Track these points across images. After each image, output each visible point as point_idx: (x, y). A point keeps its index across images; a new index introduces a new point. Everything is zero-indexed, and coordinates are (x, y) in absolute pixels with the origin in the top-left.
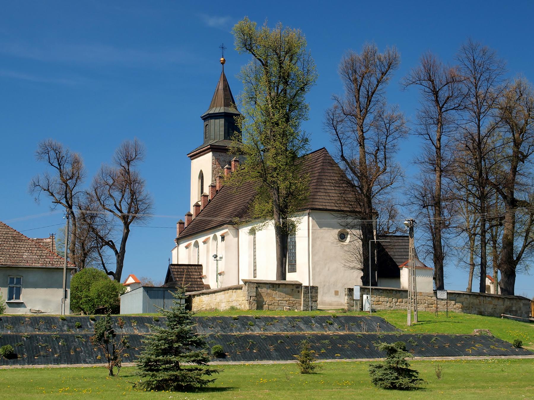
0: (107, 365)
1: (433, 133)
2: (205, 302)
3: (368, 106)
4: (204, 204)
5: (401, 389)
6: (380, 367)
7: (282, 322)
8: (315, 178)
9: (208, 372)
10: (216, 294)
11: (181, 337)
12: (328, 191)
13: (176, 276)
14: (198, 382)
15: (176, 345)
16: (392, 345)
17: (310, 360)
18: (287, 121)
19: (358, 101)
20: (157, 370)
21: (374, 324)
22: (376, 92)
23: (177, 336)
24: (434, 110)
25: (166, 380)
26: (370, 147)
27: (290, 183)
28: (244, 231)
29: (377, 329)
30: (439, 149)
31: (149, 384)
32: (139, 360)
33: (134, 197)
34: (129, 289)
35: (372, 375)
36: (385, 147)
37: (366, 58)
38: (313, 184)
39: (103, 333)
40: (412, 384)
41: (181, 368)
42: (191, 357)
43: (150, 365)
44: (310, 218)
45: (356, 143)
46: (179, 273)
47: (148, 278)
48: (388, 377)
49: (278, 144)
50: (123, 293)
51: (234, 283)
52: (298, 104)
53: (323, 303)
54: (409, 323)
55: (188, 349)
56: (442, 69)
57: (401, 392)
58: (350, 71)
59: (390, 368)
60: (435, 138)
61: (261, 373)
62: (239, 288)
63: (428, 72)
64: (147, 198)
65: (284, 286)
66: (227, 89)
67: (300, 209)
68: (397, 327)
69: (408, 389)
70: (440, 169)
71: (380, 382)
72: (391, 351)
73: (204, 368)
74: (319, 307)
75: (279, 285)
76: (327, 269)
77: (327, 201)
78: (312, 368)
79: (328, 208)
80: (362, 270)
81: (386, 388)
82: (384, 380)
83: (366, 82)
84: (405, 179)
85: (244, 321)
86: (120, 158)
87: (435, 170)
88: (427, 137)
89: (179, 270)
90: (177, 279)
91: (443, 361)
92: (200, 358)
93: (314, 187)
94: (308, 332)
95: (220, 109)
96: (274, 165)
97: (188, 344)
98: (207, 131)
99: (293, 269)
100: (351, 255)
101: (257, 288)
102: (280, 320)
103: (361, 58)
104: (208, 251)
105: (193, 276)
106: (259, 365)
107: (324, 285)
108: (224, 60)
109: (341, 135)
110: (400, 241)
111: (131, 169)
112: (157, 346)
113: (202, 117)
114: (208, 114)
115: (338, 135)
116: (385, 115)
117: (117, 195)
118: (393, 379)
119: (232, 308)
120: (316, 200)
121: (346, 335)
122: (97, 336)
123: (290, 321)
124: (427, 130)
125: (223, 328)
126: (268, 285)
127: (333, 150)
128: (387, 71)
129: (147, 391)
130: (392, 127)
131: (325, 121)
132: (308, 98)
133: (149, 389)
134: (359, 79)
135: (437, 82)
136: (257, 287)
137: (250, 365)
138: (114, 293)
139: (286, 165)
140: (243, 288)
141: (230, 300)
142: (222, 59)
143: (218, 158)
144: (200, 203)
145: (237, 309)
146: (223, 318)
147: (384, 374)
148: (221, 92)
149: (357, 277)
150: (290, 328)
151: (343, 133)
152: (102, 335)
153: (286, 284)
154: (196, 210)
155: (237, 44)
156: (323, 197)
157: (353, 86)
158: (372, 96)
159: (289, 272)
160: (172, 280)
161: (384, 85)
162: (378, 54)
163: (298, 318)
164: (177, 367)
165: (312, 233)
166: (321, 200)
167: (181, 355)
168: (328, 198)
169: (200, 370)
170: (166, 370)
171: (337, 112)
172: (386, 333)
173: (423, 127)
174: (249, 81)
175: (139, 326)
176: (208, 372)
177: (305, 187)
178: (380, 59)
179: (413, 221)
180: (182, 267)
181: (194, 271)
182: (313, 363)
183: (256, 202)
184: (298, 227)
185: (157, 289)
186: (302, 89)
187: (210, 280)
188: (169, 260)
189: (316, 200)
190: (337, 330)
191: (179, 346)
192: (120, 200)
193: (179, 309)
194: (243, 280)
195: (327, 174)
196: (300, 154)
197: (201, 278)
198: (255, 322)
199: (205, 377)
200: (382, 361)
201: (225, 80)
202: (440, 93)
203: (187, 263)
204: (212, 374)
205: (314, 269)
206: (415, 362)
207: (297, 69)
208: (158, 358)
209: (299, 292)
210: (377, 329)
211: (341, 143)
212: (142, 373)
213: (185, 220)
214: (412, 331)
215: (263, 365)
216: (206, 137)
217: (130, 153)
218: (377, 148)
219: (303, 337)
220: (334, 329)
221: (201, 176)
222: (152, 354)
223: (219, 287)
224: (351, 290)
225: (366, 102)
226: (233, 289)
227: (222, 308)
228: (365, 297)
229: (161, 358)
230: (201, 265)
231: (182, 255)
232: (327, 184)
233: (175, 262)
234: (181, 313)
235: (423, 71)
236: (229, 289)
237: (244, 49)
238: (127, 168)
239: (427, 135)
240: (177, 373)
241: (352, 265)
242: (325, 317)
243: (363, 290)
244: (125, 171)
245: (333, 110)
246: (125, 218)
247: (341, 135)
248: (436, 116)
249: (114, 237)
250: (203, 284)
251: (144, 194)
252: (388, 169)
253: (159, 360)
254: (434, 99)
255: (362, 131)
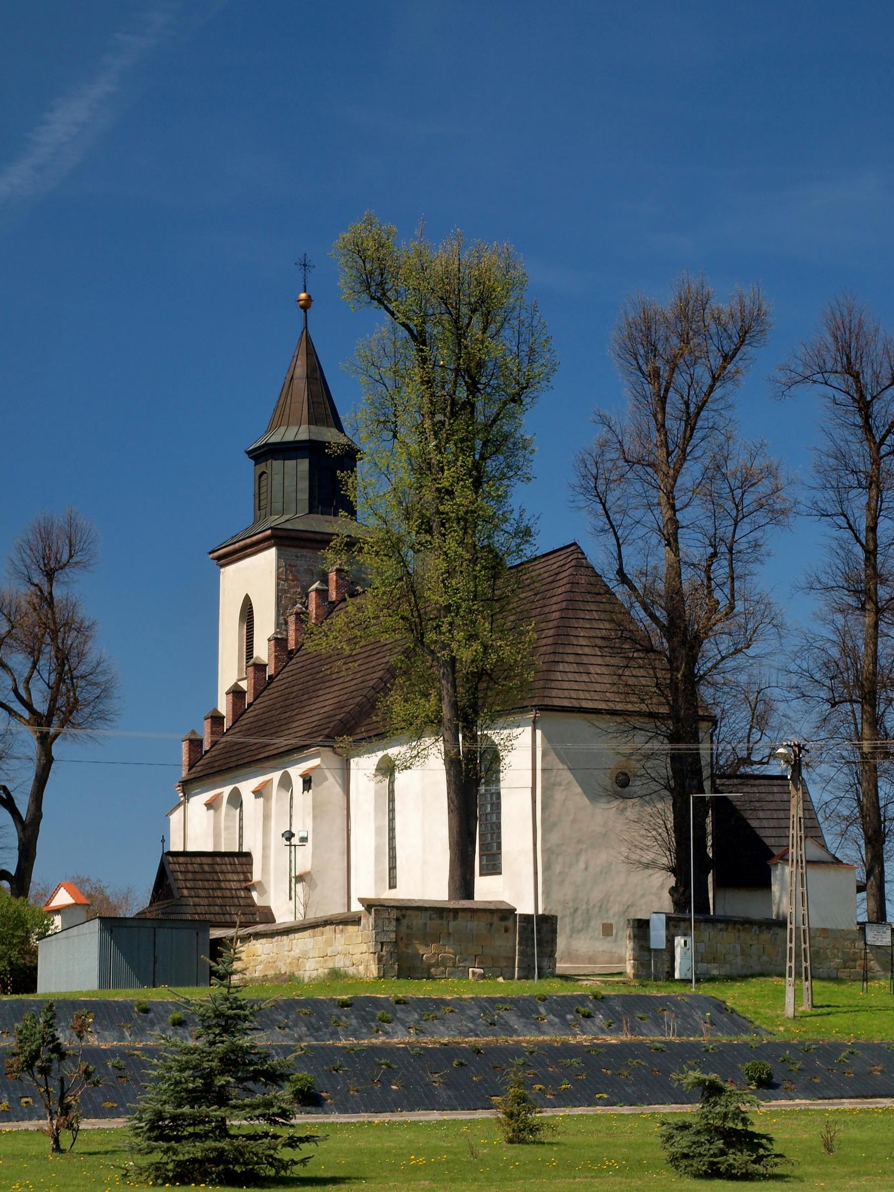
0: (45, 1124)
1: (857, 513)
2: (264, 957)
3: (687, 439)
4: (255, 689)
5: (730, 1176)
6: (684, 1127)
7: (462, 1011)
8: (551, 625)
9: (293, 1142)
10: (292, 936)
11: (233, 1061)
12: (585, 660)
13: (182, 884)
14: (271, 1165)
15: (220, 1081)
16: (713, 1076)
17: (530, 1111)
18: (477, 484)
19: (661, 427)
20: (178, 1139)
21: (697, 1015)
22: (709, 405)
23: (221, 1060)
24: (858, 451)
25: (194, 1161)
26: (693, 548)
27: (485, 647)
28: (363, 766)
29: (704, 1027)
30: (871, 553)
31: (158, 1167)
32: (137, 1115)
33: (67, 668)
34: (58, 920)
35: (667, 1146)
36: (730, 550)
37: (683, 315)
38: (544, 642)
39: (37, 1051)
40: (757, 1166)
41: (232, 1132)
42: (254, 1107)
43: (160, 1127)
44: (539, 733)
45: (655, 538)
46: (190, 876)
47: (94, 879)
48: (701, 1150)
49: (454, 545)
50: (42, 936)
51: (336, 909)
52: (506, 437)
53: (571, 956)
54: (790, 1011)
55: (247, 1090)
56: (880, 346)
57: (730, 1185)
58: (640, 347)
59: (709, 1129)
60: (862, 524)
61: (410, 1141)
62: (350, 920)
63: (845, 350)
64: (99, 669)
65: (469, 914)
66: (316, 375)
67: (510, 711)
68: (757, 1023)
69: (747, 1177)
70: (876, 603)
71: (685, 1162)
72: (712, 1091)
73: (285, 1133)
74: (561, 967)
75: (456, 912)
76: (582, 865)
77: (583, 686)
78: (533, 1130)
79: (584, 704)
80: (673, 870)
81: (698, 1176)
82: (693, 1157)
83: (680, 380)
84: (783, 632)
85: (365, 1010)
86: (28, 561)
87: (863, 608)
88: (841, 521)
89: (190, 868)
90: (185, 892)
91: (854, 1109)
92: (275, 1110)
93: (549, 649)
94: (528, 1038)
95: (299, 432)
96: (443, 601)
97: (246, 1079)
98: (263, 490)
99: (493, 867)
100: (643, 832)
101: (398, 920)
102: (459, 1005)
103: (670, 315)
104: (266, 817)
105: (228, 885)
106: (405, 1122)
107: (576, 910)
108: (309, 300)
109: (616, 518)
110: (775, 789)
111: (58, 592)
112: (177, 1083)
113: (249, 453)
114: (266, 444)
115: (608, 517)
116: (732, 466)
117: (19, 661)
118: (714, 1155)
119: (335, 974)
120: (553, 685)
121: (624, 1045)
122: (22, 1059)
123: (483, 1009)
124: (841, 502)
125: (313, 1030)
126: (428, 913)
127: (599, 555)
128: (737, 350)
129: (154, 1185)
130: (749, 498)
131: (575, 480)
132: (531, 423)
133: (160, 1181)
134: (665, 373)
135: (867, 378)
136: (403, 929)
137: (383, 1123)
138: (20, 933)
139: (475, 598)
140: (363, 921)
141: (329, 951)
142: (303, 295)
143: (293, 563)
144: (244, 685)
145: (346, 976)
146: (314, 1004)
147: (694, 1143)
148: (301, 385)
149: (662, 887)
150: (483, 1028)
151: (625, 513)
152: (35, 1055)
153: (473, 911)
154: (234, 704)
155: (345, 281)
156: (571, 676)
157: (649, 389)
158: (698, 414)
159: (481, 875)
160: (169, 894)
161: (729, 386)
162: (714, 306)
163: (503, 1000)
164: (222, 1130)
165: (543, 770)
166: (566, 685)
167: (233, 1102)
168: (585, 678)
169: (275, 1137)
170: (195, 1136)
171: (608, 456)
172: (725, 1039)
173: (831, 494)
174: (378, 378)
175: (100, 1024)
176: (293, 1142)
177: (523, 657)
178: (717, 320)
179: (800, 748)
180: (198, 860)
181: (229, 868)
182: (536, 1117)
183: (395, 696)
184: (506, 761)
185: (135, 923)
186: (516, 399)
187: (280, 902)
188: (163, 841)
189: (553, 685)
190: (603, 1031)
191: (228, 1082)
192: (26, 675)
193: (227, 999)
194: (362, 900)
195: (581, 615)
196: (511, 561)
197: (248, 889)
198: (394, 1013)
199: (286, 1154)
200: (690, 1111)
201: (311, 352)
202: (876, 407)
203: (210, 849)
204: (302, 1146)
205: (547, 867)
206: (765, 1115)
207: (500, 348)
208: (179, 1111)
209: (506, 930)
210: (704, 1027)
211: (617, 539)
212: (145, 1144)
213: (205, 733)
214: (795, 1033)
215: (415, 1123)
216: (261, 507)
217: (54, 549)
218: (711, 550)
219: (517, 1051)
220: (595, 1029)
221: (247, 613)
222: (165, 1102)
223: (300, 917)
224: (641, 927)
225: (682, 428)
226: (338, 924)
227: (307, 974)
228: (679, 941)
229: (186, 1109)
230: (248, 855)
231: (196, 826)
232: (582, 642)
233: (176, 846)
234: (231, 1008)
235: (833, 348)
236: (327, 923)
237: (365, 297)
238: (46, 588)
239: (842, 518)
240: (224, 1144)
241: (648, 857)
242: (573, 997)
243: (674, 924)
244: (42, 597)
245: (596, 450)
246: (39, 720)
247: (618, 516)
248: (865, 465)
249: (12, 774)
250: (253, 905)
251: (92, 657)
252: (739, 606)
253: (182, 1114)
254: (859, 420)
255: (673, 507)
